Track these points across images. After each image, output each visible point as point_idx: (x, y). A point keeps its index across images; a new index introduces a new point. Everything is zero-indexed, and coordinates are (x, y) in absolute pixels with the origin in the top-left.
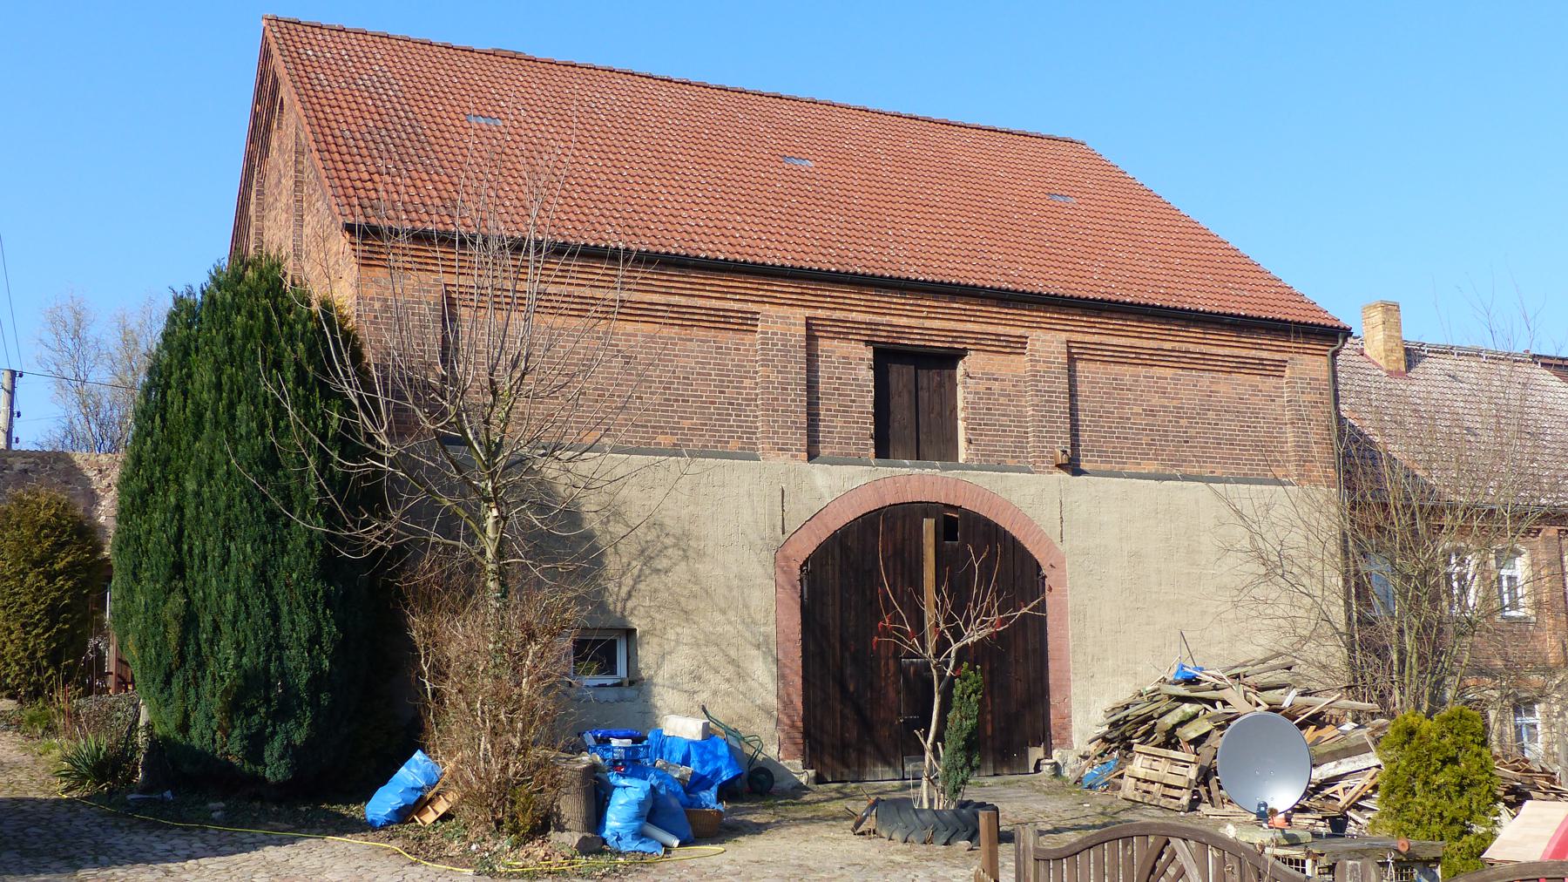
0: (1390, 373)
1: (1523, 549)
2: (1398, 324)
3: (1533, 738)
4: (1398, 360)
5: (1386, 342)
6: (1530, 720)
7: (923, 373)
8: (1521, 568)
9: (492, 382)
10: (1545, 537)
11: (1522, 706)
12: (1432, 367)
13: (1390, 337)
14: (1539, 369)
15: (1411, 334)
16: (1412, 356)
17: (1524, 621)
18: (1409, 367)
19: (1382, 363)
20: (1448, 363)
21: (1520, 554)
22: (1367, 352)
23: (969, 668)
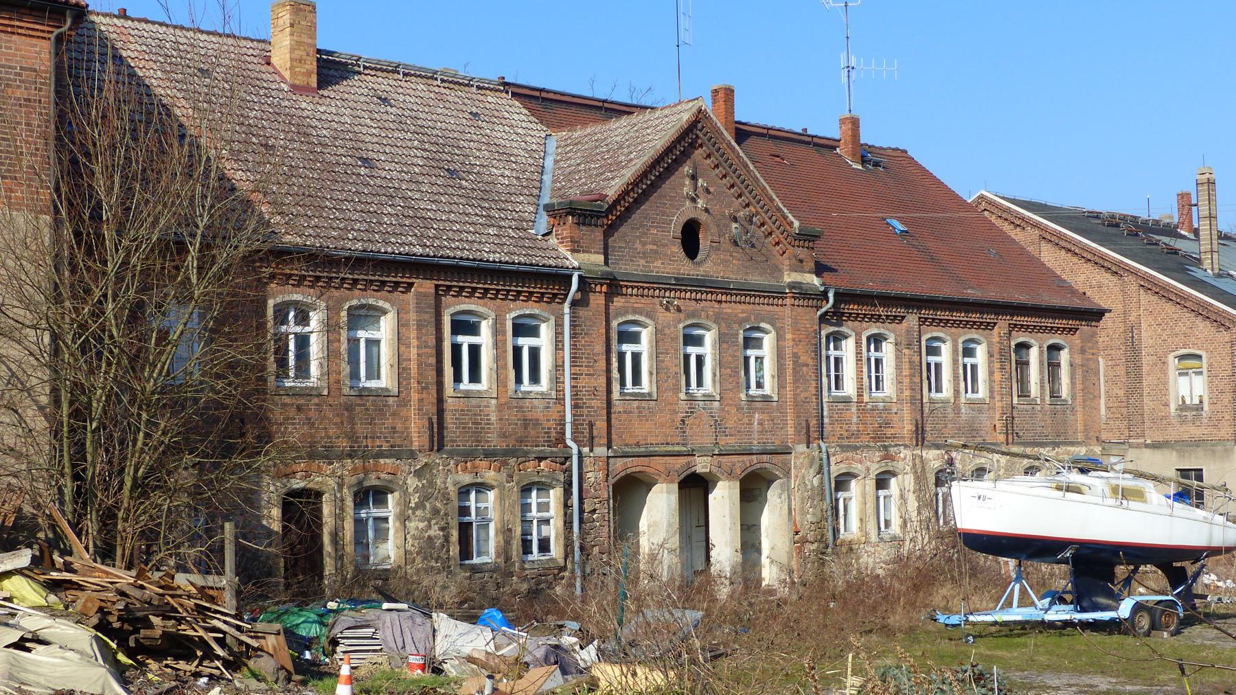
0: (295, 88)
1: (387, 306)
2: (312, 27)
3: (381, 535)
4: (309, 74)
5: (292, 50)
6: (376, 512)
7: (1024, 562)
8: (385, 329)
9: (16, 412)
10: (418, 294)
11: (370, 495)
12: (355, 89)
13: (299, 43)
14: (506, 99)
15: (336, 38)
16: (331, 70)
17: (382, 394)
18: (320, 87)
19: (287, 75)
20: (383, 84)
21: (385, 312)
22: (273, 61)
23: (61, 556)
